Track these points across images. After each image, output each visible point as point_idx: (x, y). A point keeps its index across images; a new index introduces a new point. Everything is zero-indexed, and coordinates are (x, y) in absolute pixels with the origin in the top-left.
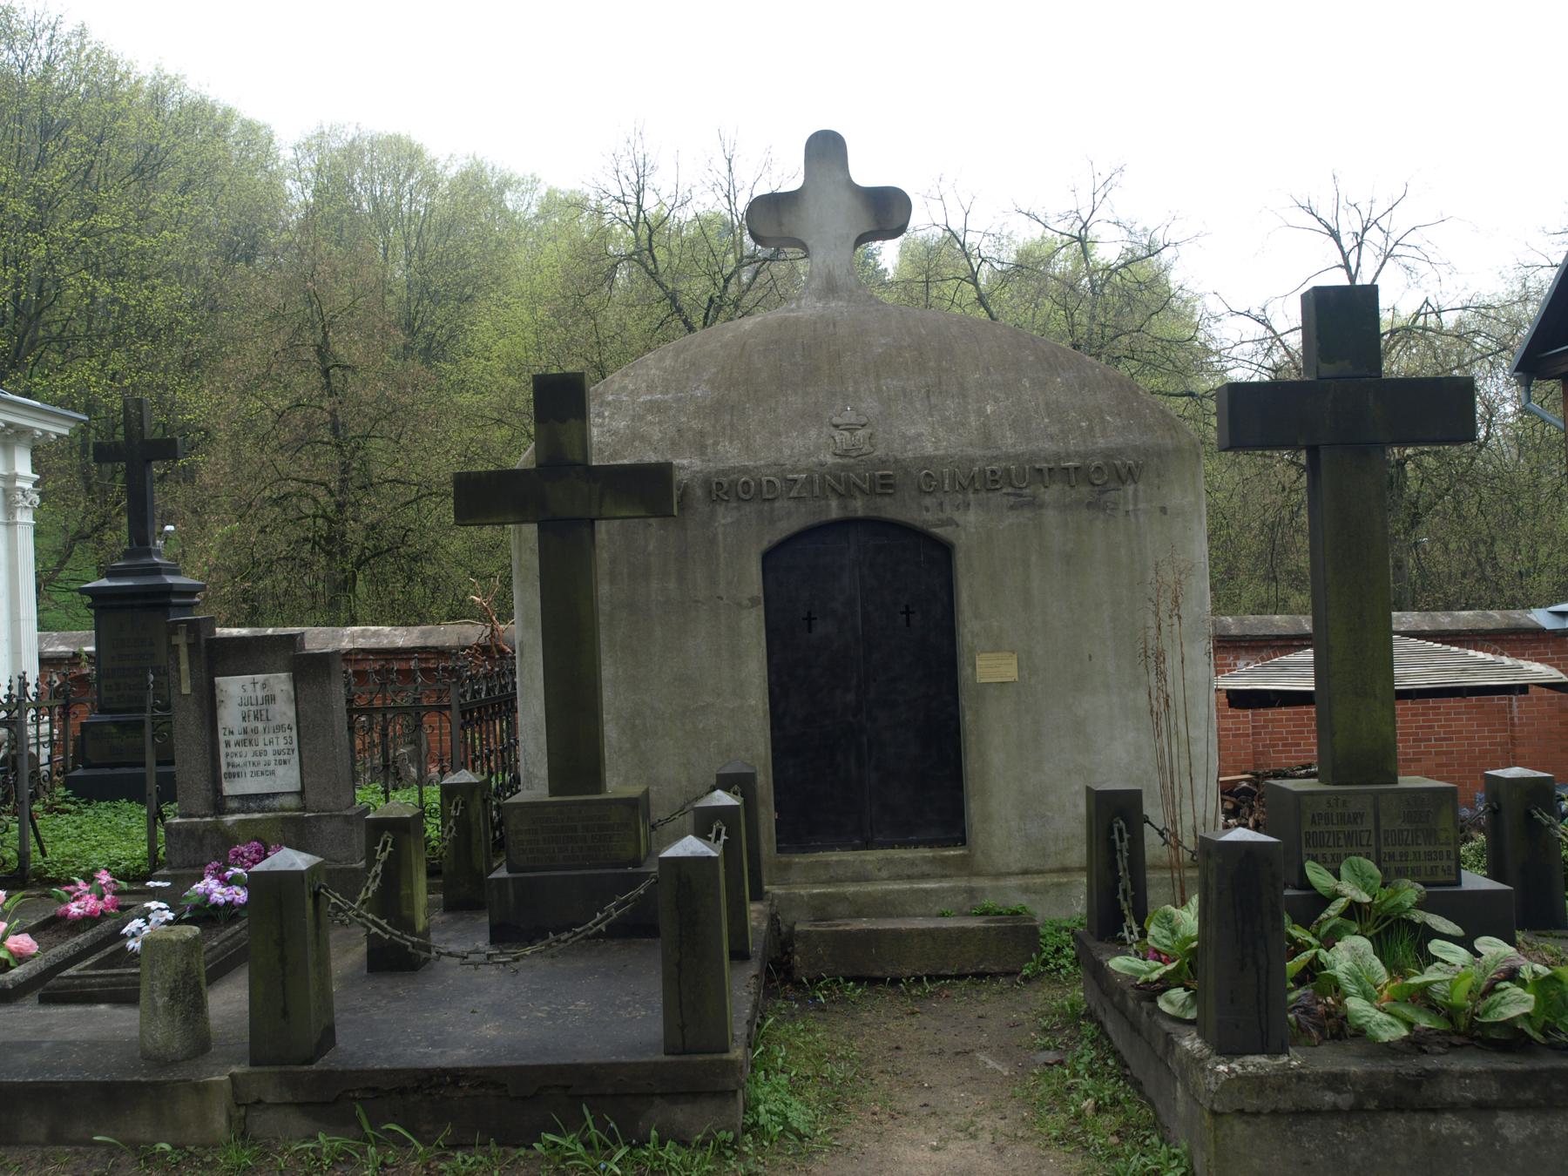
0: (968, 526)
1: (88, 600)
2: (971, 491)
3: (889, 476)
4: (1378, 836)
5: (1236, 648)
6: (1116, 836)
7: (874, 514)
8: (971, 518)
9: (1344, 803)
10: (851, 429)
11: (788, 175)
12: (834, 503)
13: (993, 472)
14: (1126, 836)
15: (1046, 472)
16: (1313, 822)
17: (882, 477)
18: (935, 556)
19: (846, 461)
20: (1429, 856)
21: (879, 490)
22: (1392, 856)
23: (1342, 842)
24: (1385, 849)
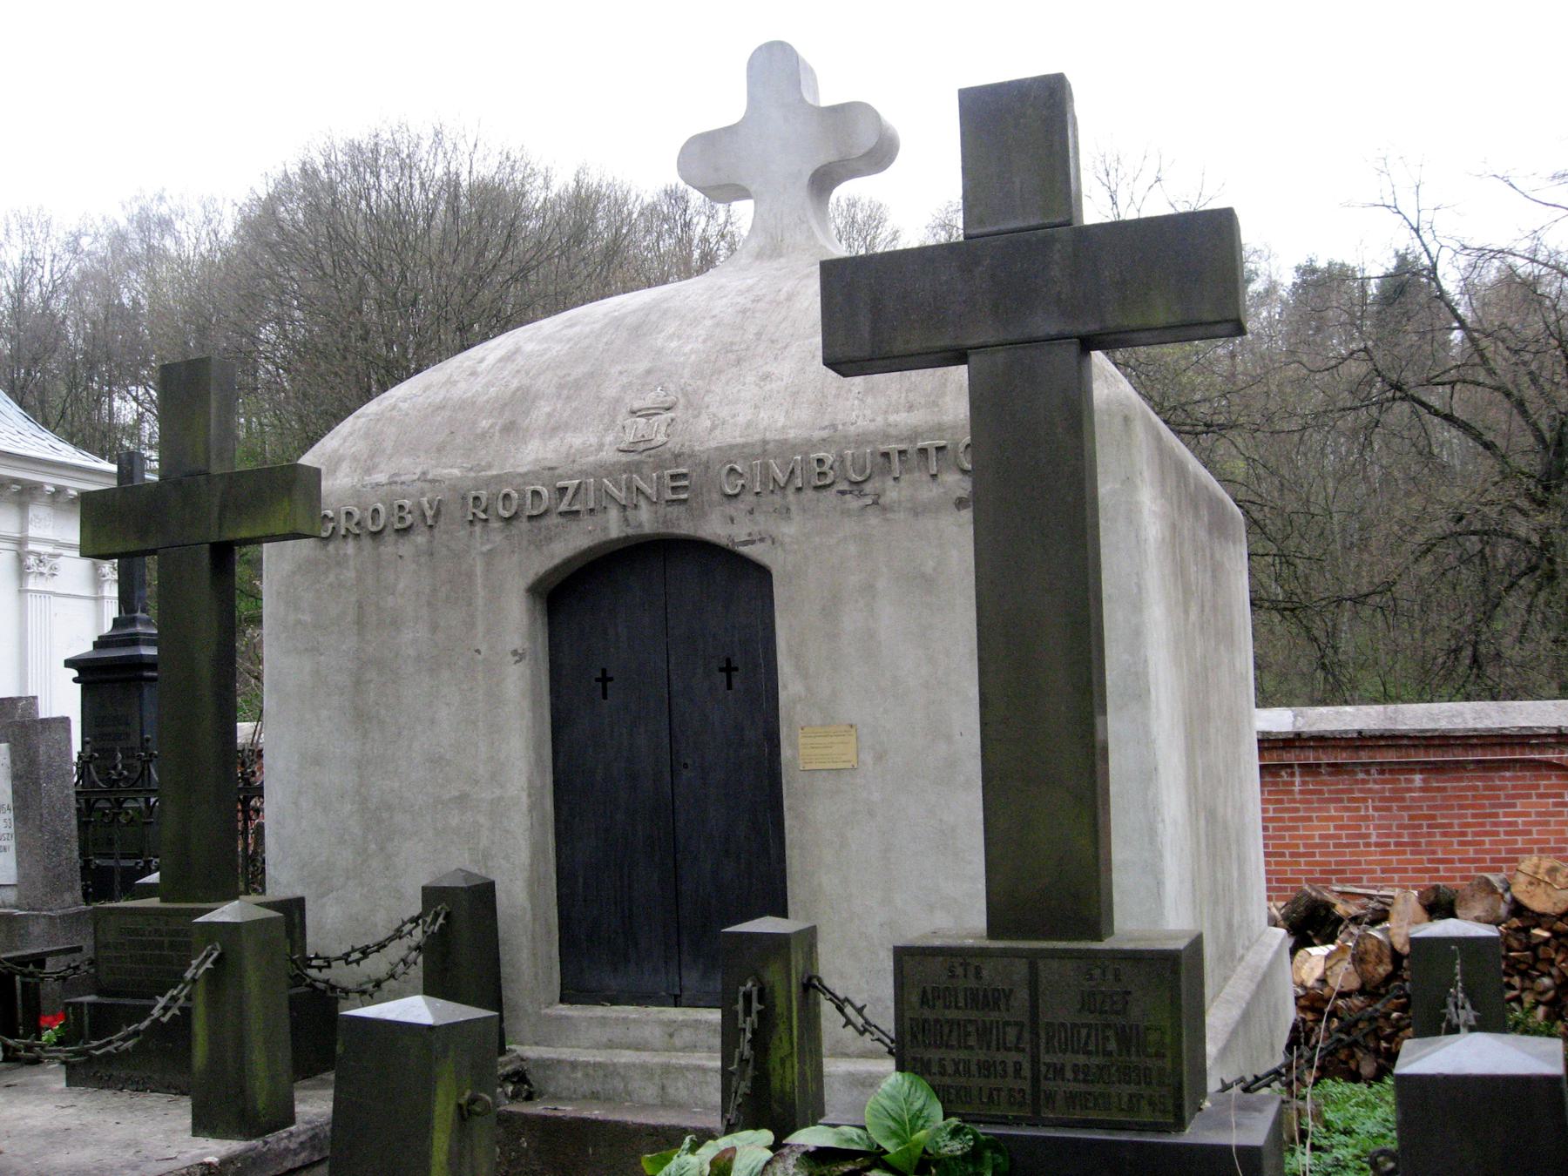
0: (791, 545)
1: (75, 673)
2: (790, 490)
3: (684, 476)
4: (1035, 1034)
5: (1512, 744)
6: (740, 1006)
7: (662, 530)
8: (788, 530)
9: (978, 970)
10: (648, 414)
11: (725, 104)
12: (614, 513)
13: (820, 461)
14: (756, 1006)
15: (895, 458)
16: (924, 1001)
17: (674, 477)
18: (740, 580)
19: (636, 457)
20: (986, 1068)
21: (669, 495)
22: (1059, 1071)
23: (972, 1041)
24: (1046, 1058)
